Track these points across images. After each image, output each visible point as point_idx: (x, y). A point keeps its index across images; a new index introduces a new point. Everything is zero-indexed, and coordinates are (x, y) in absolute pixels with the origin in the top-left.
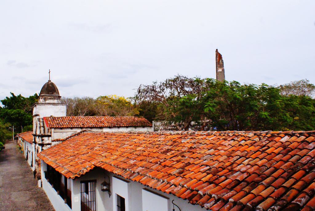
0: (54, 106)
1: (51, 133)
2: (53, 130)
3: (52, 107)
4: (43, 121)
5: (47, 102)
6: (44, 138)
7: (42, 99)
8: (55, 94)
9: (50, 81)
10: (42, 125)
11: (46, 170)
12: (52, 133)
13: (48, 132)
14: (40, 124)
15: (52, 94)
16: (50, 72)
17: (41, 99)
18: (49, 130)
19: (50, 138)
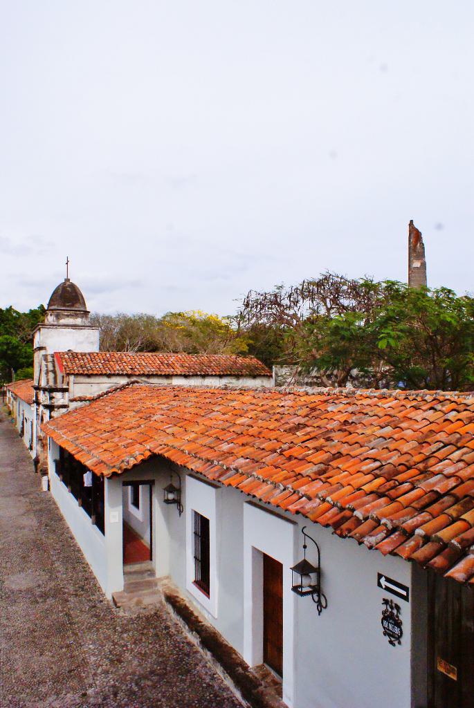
1: (68, 384)
2: (72, 378)
3: (70, 332)
4: (54, 361)
5: (62, 321)
6: (55, 393)
7: (51, 315)
8: (78, 307)
9: (67, 280)
10: (51, 368)
11: (58, 458)
12: (71, 384)
13: (63, 383)
14: (47, 366)
15: (73, 306)
16: (68, 261)
19: (67, 394)
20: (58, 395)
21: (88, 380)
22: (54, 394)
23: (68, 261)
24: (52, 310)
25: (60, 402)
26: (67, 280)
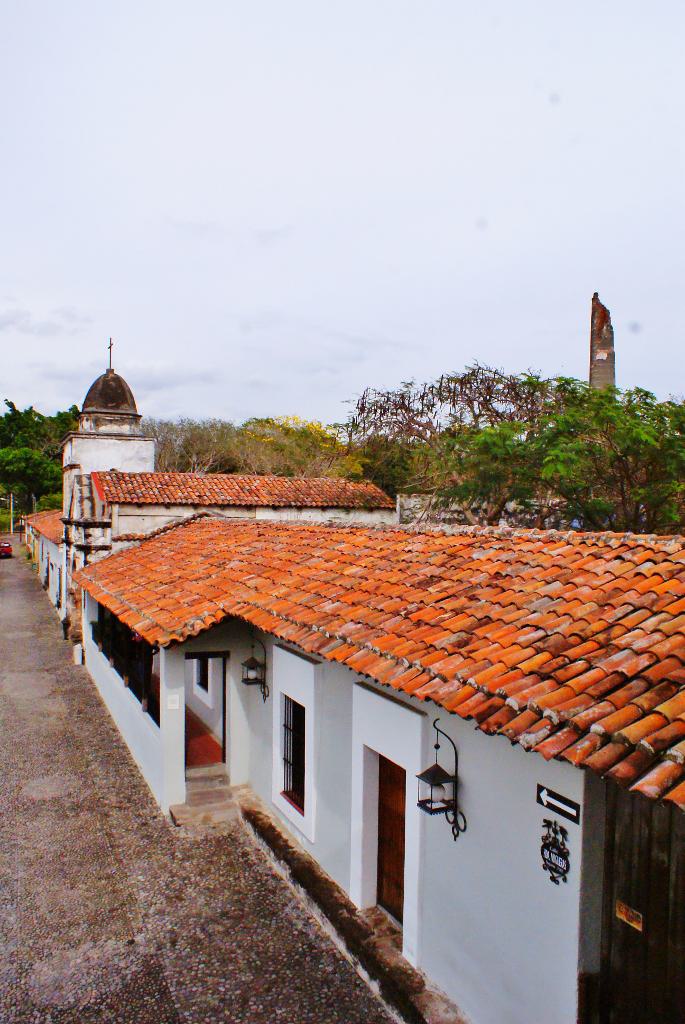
0: (120, 442)
1: (110, 517)
2: (116, 509)
4: (90, 484)
5: (103, 429)
7: (87, 420)
8: (124, 409)
9: (110, 371)
10: (86, 493)
11: (96, 619)
12: (115, 517)
13: (103, 514)
15: (117, 407)
16: (111, 345)
17: (85, 421)
18: (106, 510)
19: (108, 530)
20: (96, 532)
21: (138, 511)
22: (91, 531)
23: (111, 345)
24: (89, 413)
25: (100, 542)
26: (110, 371)
